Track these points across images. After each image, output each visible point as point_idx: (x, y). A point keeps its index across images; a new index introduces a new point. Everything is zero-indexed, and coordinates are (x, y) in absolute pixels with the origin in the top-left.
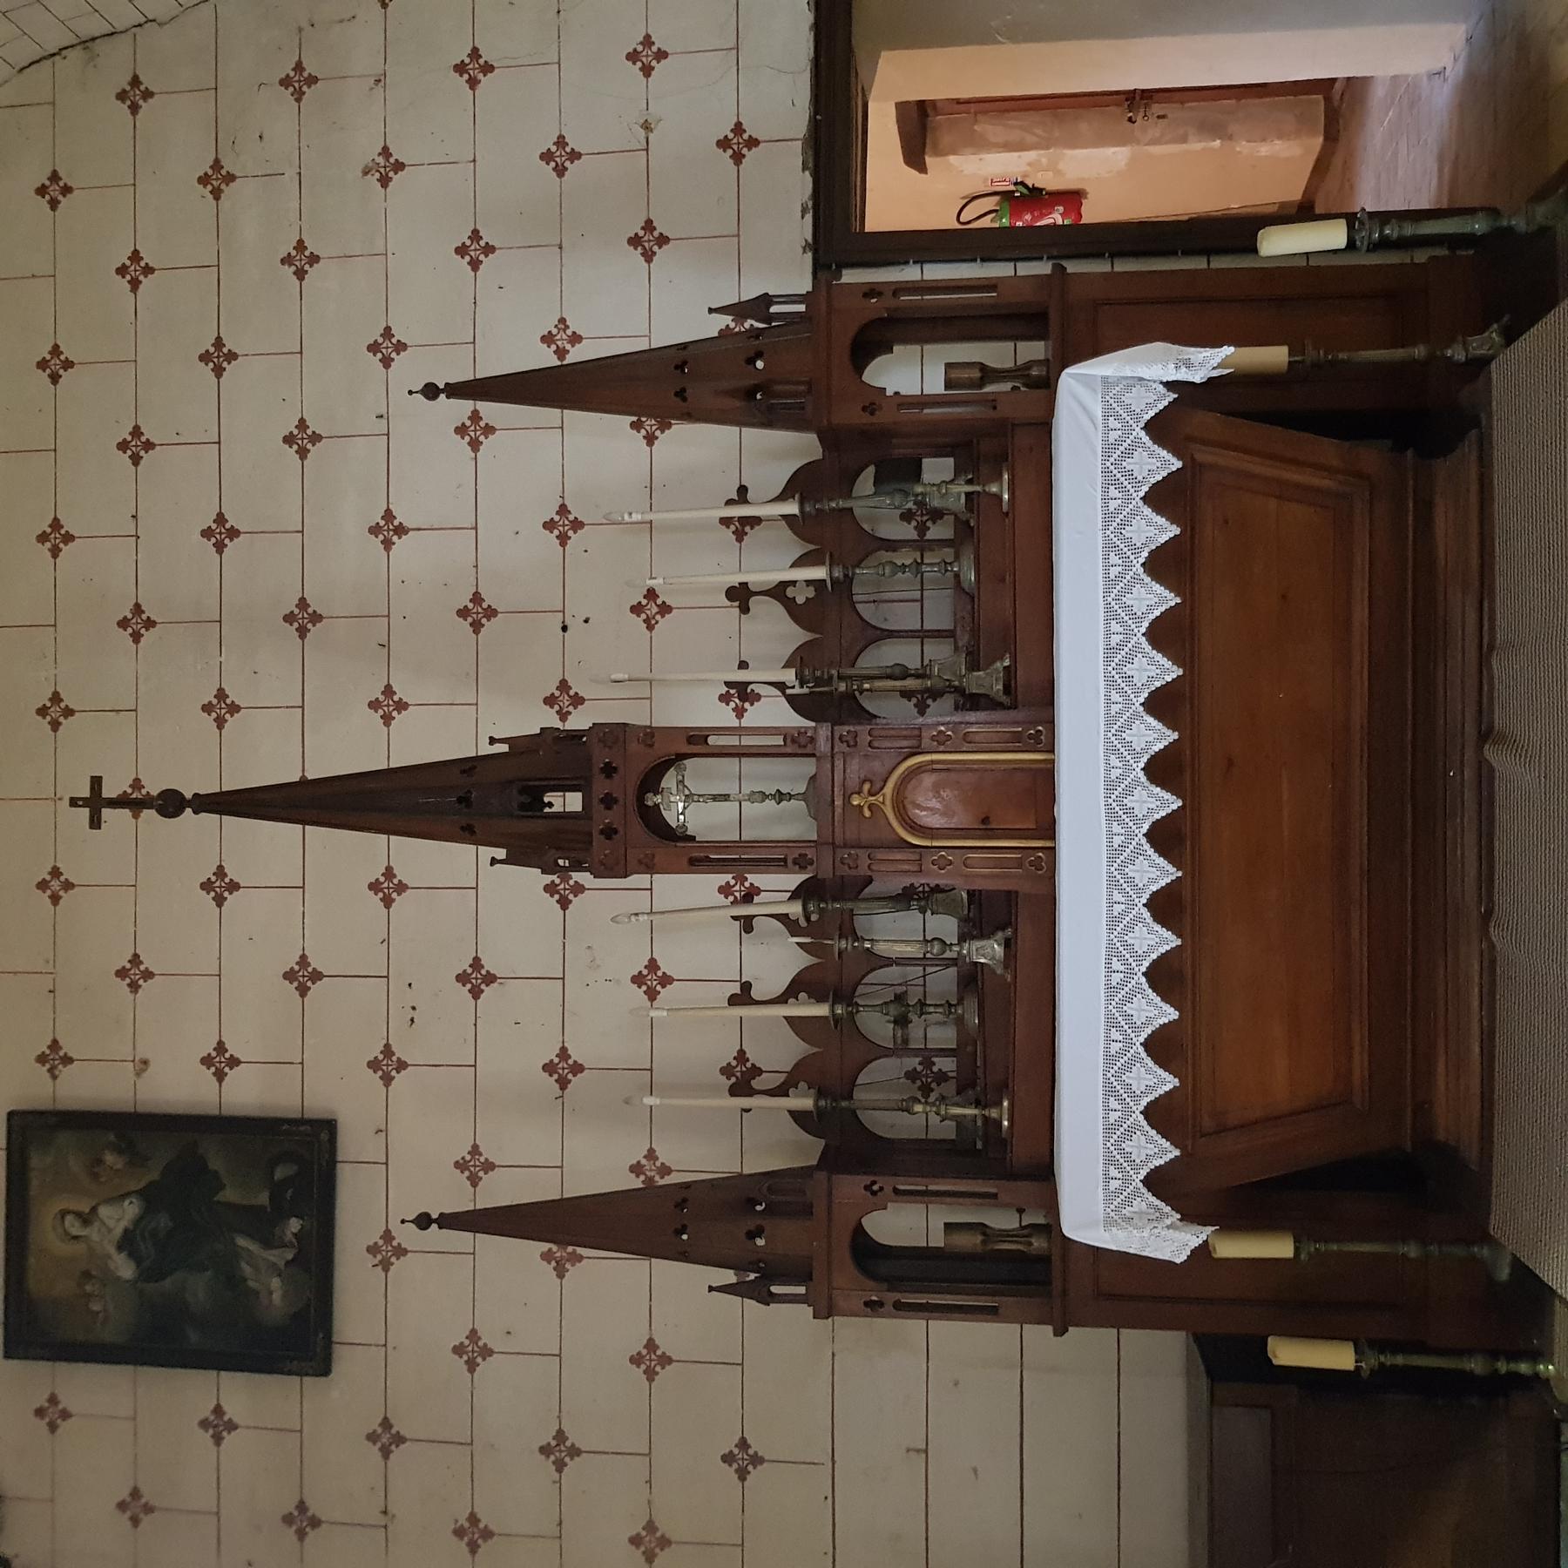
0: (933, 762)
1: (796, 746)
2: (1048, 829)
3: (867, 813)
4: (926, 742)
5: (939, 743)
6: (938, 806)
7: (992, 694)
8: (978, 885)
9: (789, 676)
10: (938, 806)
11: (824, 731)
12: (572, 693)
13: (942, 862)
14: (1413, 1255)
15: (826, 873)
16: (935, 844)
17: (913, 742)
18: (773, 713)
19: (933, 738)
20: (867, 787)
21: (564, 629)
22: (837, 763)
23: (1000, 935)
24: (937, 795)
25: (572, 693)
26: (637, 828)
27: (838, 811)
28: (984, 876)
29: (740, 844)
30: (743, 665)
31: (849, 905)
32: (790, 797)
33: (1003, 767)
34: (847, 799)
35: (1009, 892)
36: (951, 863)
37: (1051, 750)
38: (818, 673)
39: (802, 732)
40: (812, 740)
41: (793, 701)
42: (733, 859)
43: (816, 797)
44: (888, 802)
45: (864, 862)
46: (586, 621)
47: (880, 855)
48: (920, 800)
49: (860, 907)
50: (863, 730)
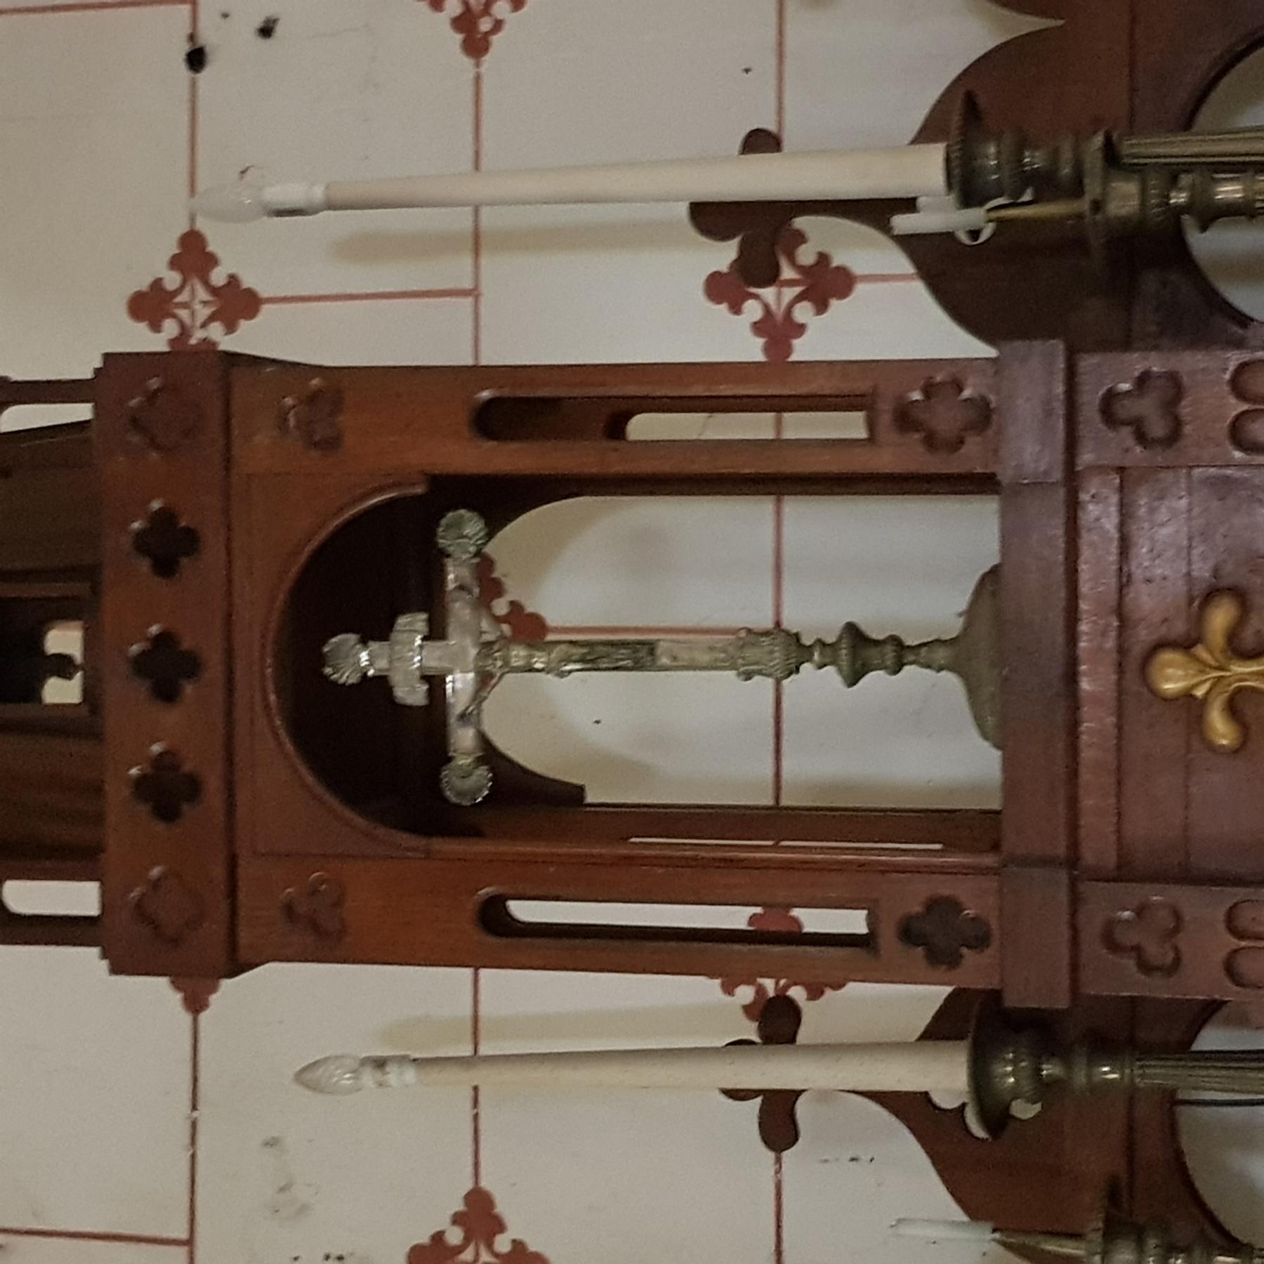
1: (915, 442)
3: (1221, 729)
9: (926, 171)
11: (1036, 374)
12: (218, 277)
14: (992, 150)
15: (1037, 985)
18: (890, 320)
20: (1221, 617)
21: (196, 59)
22: (1091, 511)
25: (218, 277)
26: (276, 781)
27: (1096, 723)
29: (775, 820)
30: (761, 142)
31: (1157, 1074)
32: (899, 653)
34: (1134, 664)
38: (1034, 159)
39: (940, 379)
40: (983, 416)
41: (937, 262)
42: (744, 885)
43: (1012, 653)
45: (1207, 944)
46: (266, 31)
49: (1208, 1086)
50: (1208, 371)
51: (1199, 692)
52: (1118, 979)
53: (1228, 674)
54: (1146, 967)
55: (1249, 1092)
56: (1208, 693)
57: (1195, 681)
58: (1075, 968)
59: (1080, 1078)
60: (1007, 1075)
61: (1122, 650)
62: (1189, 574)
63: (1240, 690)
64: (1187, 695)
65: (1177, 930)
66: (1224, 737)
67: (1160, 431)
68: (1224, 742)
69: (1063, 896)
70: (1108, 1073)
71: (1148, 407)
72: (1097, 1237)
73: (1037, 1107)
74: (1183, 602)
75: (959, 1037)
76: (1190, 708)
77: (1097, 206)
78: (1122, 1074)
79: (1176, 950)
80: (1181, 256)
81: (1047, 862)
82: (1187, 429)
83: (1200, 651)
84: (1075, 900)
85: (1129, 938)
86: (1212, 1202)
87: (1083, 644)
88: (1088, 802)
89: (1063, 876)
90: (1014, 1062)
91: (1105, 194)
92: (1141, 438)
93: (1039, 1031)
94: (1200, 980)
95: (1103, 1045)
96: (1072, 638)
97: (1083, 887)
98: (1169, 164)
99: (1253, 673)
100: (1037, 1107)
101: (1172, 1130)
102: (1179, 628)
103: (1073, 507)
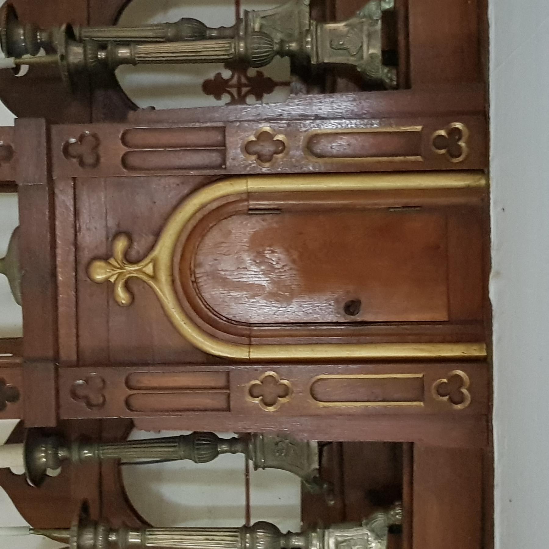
0: (250, 195)
2: (474, 321)
3: (122, 295)
4: (236, 157)
5: (260, 158)
6: (263, 281)
7: (361, 65)
8: (337, 434)
10: (263, 281)
13: (270, 391)
14: (22, 32)
16: (256, 354)
17: (214, 158)
19: (247, 148)
20: (121, 245)
23: (381, 519)
24: (259, 258)
27: (65, 295)
28: (351, 416)
31: (110, 452)
33: (384, 202)
34: (82, 268)
35: (395, 444)
36: (286, 392)
37: (480, 165)
38: (41, 37)
44: (164, 276)
45: (118, 394)
47: (150, 378)
48: (226, 266)
49: (127, 454)
50: (111, 136)
51: (112, 280)
52: (78, 413)
53: (125, 271)
54: (90, 405)
55: (150, 457)
56: (116, 279)
57: (110, 274)
58: (58, 406)
59: (75, 457)
60: (42, 458)
61: (76, 261)
62: (107, 226)
63: (128, 279)
64: (107, 281)
65: (104, 387)
66: (124, 299)
67: (89, 162)
68: (123, 302)
69: (52, 375)
70: (87, 453)
71: (84, 150)
72: (74, 529)
73: (59, 471)
74: (104, 239)
75: (21, 442)
76: (108, 286)
77: (63, 57)
78: (94, 454)
79: (104, 397)
80: (115, 85)
81: (45, 360)
82: (102, 160)
83: (112, 261)
84: (57, 376)
85: (81, 392)
86: (137, 506)
87: (59, 259)
88: (62, 332)
89: (51, 366)
90: (45, 452)
91: (67, 51)
92: (82, 163)
93: (59, 435)
94: (115, 411)
95: (86, 441)
96: (54, 256)
97: (61, 371)
98: (98, 41)
99: (135, 270)
100: (59, 471)
101: (119, 475)
102: (102, 251)
103: (52, 195)
